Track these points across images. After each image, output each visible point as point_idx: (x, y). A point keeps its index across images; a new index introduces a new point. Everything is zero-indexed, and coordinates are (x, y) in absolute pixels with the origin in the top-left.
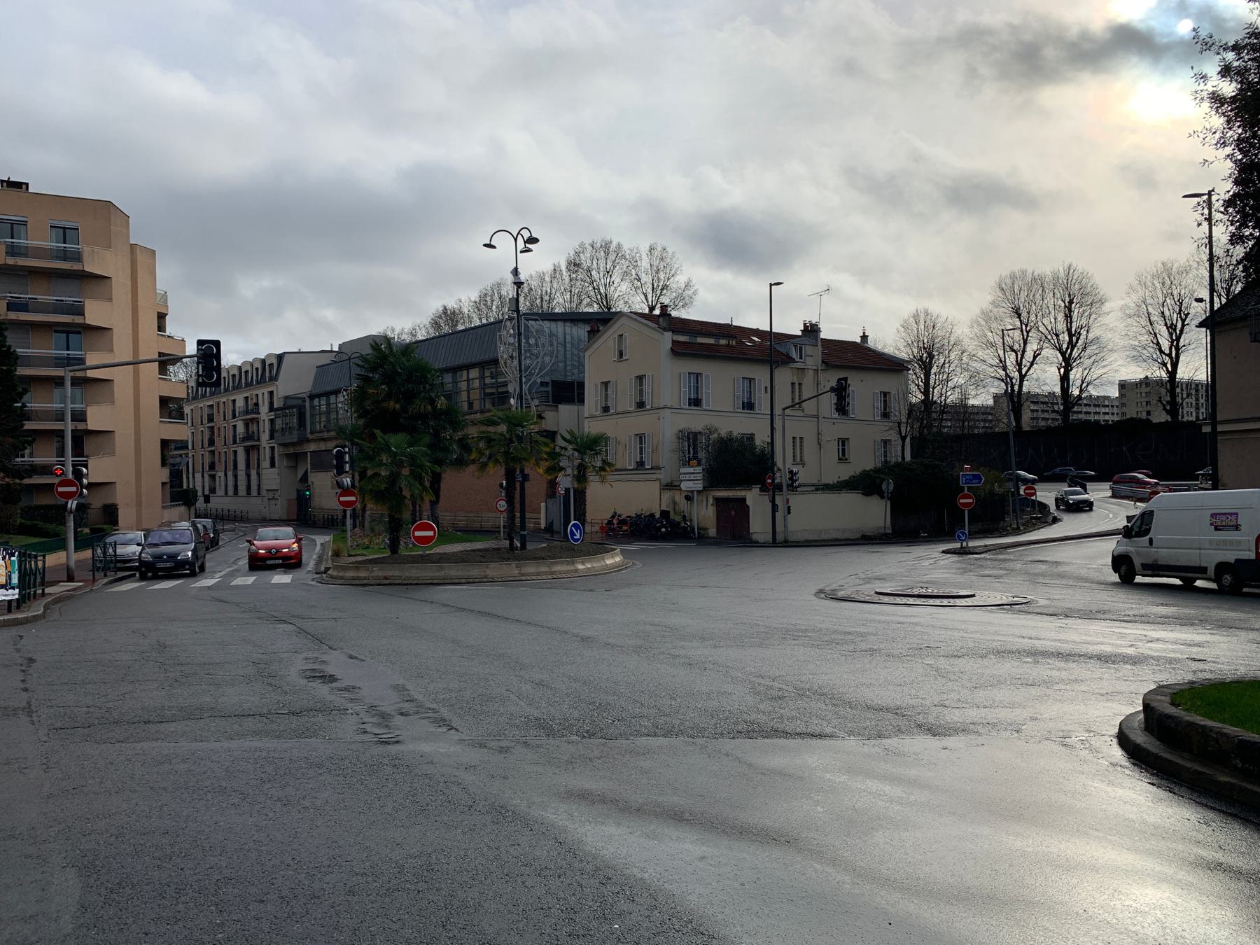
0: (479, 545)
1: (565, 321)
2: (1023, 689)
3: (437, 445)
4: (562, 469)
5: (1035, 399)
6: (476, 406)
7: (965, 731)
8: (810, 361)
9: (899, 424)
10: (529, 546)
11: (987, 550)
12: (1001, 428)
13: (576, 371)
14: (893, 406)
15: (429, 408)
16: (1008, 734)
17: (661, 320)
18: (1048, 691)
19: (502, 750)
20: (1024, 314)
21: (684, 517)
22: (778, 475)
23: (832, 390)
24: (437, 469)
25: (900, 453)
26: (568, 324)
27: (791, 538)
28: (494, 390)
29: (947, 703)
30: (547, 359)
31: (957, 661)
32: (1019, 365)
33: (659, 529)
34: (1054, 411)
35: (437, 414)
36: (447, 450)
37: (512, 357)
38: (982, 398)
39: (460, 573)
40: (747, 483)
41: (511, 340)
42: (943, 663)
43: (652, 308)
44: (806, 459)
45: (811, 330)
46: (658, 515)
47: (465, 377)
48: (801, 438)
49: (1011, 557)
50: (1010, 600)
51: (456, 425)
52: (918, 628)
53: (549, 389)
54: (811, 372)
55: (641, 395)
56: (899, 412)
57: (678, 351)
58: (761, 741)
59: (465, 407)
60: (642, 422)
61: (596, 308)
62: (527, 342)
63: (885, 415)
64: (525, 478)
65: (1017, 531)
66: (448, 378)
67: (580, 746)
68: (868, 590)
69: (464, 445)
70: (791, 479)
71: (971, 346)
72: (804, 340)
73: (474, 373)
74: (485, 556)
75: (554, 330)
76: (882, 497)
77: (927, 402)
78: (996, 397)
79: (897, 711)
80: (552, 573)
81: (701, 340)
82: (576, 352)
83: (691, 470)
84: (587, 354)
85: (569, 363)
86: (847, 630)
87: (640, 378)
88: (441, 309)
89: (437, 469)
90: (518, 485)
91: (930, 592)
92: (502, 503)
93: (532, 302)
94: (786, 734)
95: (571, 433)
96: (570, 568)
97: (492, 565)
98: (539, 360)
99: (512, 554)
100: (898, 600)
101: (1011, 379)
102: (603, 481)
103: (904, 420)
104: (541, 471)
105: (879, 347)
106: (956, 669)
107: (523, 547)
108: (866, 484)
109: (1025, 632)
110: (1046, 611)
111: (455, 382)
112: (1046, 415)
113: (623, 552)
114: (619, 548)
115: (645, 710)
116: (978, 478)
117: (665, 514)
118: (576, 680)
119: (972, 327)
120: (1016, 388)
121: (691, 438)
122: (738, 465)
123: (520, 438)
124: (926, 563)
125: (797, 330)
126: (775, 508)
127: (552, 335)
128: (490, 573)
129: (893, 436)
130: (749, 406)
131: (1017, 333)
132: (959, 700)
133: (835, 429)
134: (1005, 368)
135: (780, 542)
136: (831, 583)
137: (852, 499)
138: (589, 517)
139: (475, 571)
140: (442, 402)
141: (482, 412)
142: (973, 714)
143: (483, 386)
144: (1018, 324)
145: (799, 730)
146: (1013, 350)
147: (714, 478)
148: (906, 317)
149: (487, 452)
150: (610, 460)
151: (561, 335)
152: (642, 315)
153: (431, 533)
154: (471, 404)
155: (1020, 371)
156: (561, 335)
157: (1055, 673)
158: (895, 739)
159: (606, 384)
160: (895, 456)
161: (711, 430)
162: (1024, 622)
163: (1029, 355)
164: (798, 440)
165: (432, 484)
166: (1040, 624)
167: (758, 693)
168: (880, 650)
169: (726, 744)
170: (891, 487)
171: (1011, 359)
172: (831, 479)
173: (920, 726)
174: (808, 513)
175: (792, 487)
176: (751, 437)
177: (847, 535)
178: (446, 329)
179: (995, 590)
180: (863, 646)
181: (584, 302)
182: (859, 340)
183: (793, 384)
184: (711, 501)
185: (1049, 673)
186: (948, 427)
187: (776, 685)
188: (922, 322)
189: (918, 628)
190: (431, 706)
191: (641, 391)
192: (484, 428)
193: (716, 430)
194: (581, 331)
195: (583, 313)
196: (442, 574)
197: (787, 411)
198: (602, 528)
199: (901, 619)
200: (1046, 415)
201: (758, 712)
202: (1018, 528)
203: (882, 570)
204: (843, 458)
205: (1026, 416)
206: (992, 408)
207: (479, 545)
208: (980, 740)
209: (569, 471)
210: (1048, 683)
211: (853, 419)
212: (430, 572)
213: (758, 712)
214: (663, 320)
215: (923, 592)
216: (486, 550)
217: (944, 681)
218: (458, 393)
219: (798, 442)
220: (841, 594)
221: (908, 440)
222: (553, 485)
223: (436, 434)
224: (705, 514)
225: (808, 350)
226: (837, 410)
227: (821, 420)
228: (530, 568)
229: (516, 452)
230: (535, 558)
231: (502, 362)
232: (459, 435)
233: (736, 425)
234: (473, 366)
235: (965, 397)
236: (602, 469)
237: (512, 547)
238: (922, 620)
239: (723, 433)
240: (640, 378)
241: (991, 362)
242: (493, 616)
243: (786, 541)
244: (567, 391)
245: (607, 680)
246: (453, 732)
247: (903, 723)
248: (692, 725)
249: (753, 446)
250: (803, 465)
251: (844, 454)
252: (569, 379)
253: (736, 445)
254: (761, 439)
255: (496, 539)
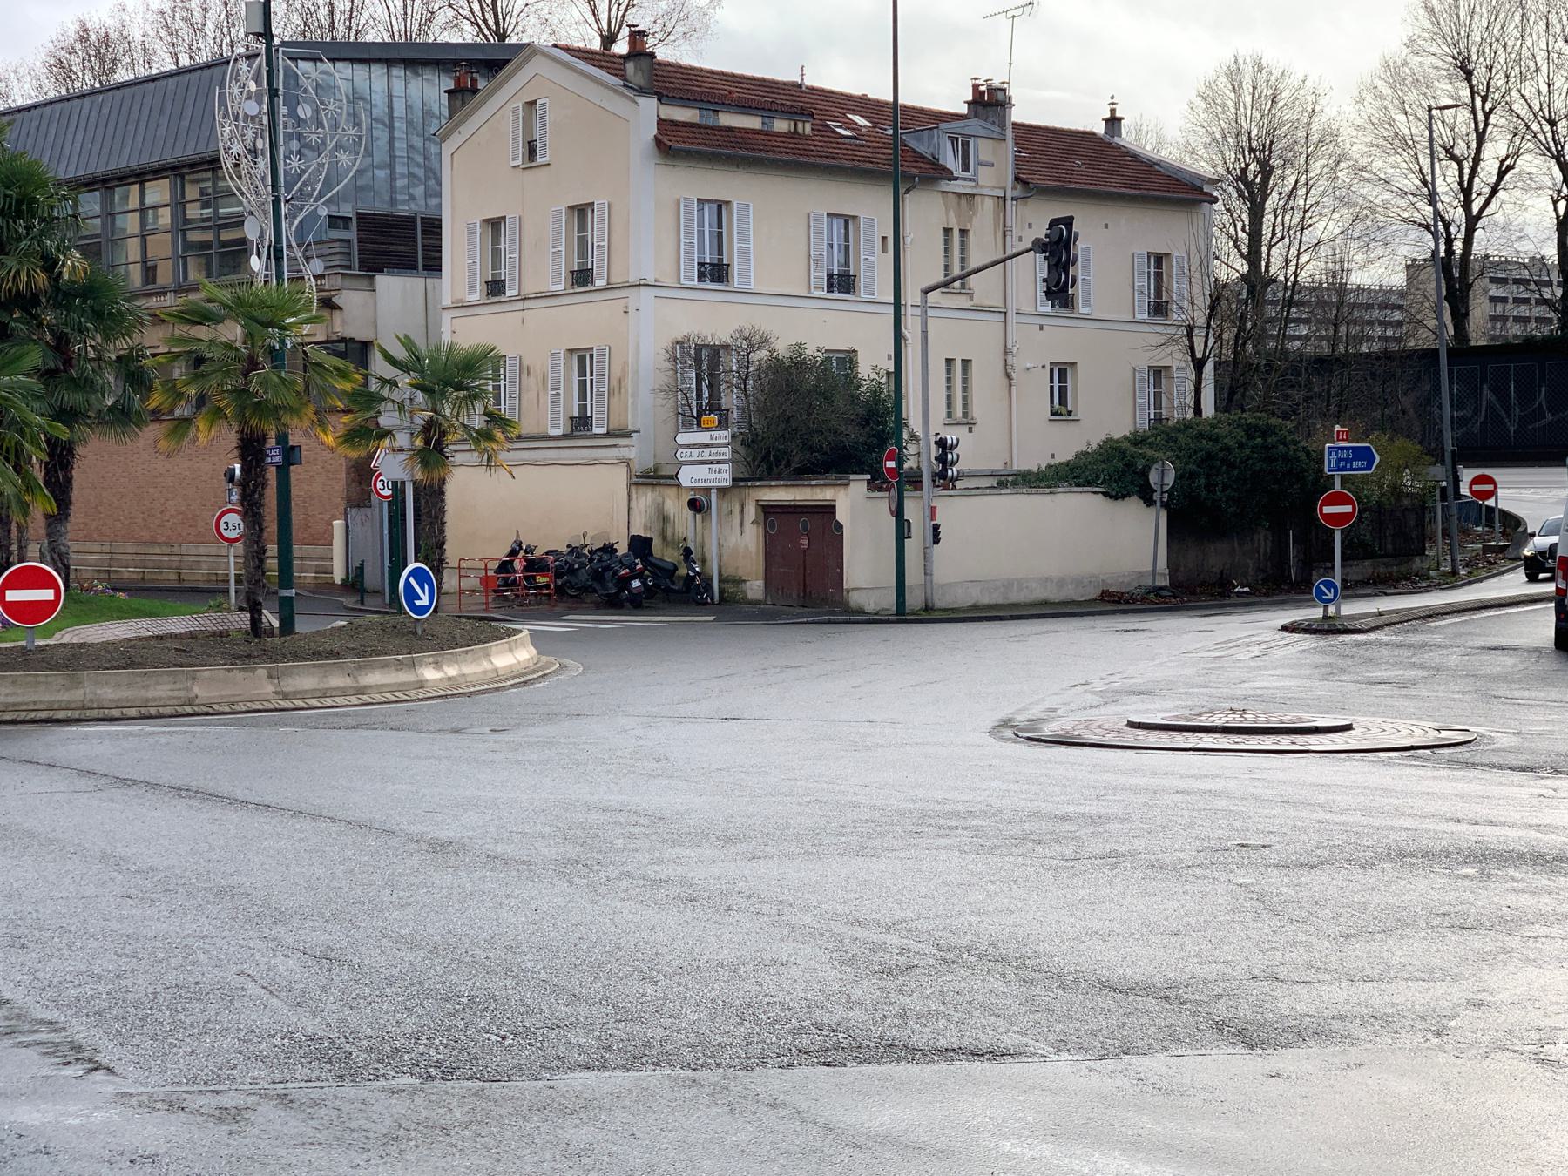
0: (174, 625)
1: (389, 63)
2: (1453, 938)
3: (61, 368)
4: (385, 434)
5: (1501, 273)
6: (164, 276)
7: (1321, 1034)
8: (986, 177)
9: (1190, 330)
10: (303, 626)
11: (1384, 622)
12: (1421, 340)
13: (419, 191)
14: (1178, 288)
15: (42, 278)
16: (1417, 1039)
17: (630, 66)
18: (1512, 942)
19: (225, 1115)
20: (1480, 74)
21: (687, 552)
22: (912, 449)
23: (1039, 246)
24: (62, 432)
25: (1190, 400)
26: (398, 72)
27: (938, 604)
28: (209, 236)
29: (1282, 972)
30: (344, 158)
31: (1307, 877)
32: (1467, 191)
33: (624, 582)
34: (1543, 301)
35: (62, 295)
36: (86, 385)
37: (253, 152)
38: (1379, 270)
39: (123, 694)
40: (838, 462)
41: (251, 108)
42: (1277, 883)
43: (609, 39)
44: (976, 412)
45: (989, 102)
46: (622, 548)
47: (134, 202)
48: (966, 362)
49: (1437, 638)
50: (1432, 737)
51: (110, 321)
52: (1221, 804)
53: (352, 234)
54: (989, 204)
55: (496, 263)
56: (1191, 303)
57: (672, 145)
58: (853, 1070)
59: (136, 276)
60: (583, 320)
61: (468, 34)
62: (292, 113)
63: (1159, 309)
64: (291, 455)
65: (1452, 580)
66: (91, 203)
67: (418, 1100)
68: (1110, 720)
69: (133, 373)
70: (942, 459)
71: (1357, 146)
72: (973, 126)
73: (158, 192)
74: (184, 652)
76: (1149, 502)
77: (1256, 280)
78: (1412, 267)
79: (1167, 993)
80: (361, 691)
81: (727, 120)
82: (418, 142)
83: (704, 437)
84: (447, 149)
85: (400, 169)
86: (1061, 810)
87: (581, 212)
88: (73, 29)
89: (62, 432)
90: (271, 474)
91: (1249, 721)
92: (234, 518)
93: (308, 15)
94: (913, 1053)
95: (407, 343)
96: (405, 677)
97: (206, 672)
98: (324, 159)
99: (263, 642)
100: (1180, 740)
101: (1447, 225)
102: (490, 462)
103: (1201, 320)
104: (329, 440)
105: (1147, 147)
106: (1306, 894)
107: (287, 626)
108: (1113, 472)
109: (1462, 809)
110: (1511, 760)
111: (109, 215)
112: (1523, 311)
113: (536, 638)
114: (526, 630)
115: (582, 1011)
116: (1365, 455)
117: (640, 545)
118: (413, 944)
119: (1361, 100)
120: (1458, 246)
121: (703, 363)
122: (816, 428)
123: (276, 356)
124: (1244, 655)
125: (955, 100)
126: (902, 530)
127: (355, 97)
128: (201, 691)
129: (1177, 359)
130: (842, 283)
131: (1464, 115)
132: (1309, 965)
133: (1044, 339)
134: (1432, 198)
135: (912, 611)
136: (1026, 705)
137: (1080, 509)
138: (452, 552)
139: (162, 689)
140: (73, 265)
141: (179, 291)
142: (1339, 996)
143: (182, 226)
144: (1465, 94)
145: (942, 1043)
146: (1453, 157)
147: (763, 457)
148: (1211, 75)
149: (192, 392)
150: (505, 410)
151: (379, 100)
153: (47, 595)
154: (150, 272)
155: (1467, 205)
156: (379, 100)
157: (1527, 900)
158: (1162, 1056)
159: (495, 224)
160: (1178, 407)
161: (753, 341)
162: (1461, 786)
163: (1489, 169)
164: (958, 364)
165: (49, 472)
166: (1496, 791)
167: (850, 961)
168: (1134, 854)
169: (771, 1081)
170: (1170, 479)
171: (1447, 180)
172: (1032, 460)
173: (1218, 1026)
174: (982, 537)
175: (944, 478)
176: (848, 359)
177: (1070, 593)
178: (87, 81)
179: (1400, 715)
180: (1095, 847)
181: (440, 19)
182: (1100, 129)
184: (751, 512)
185: (1512, 899)
186: (1303, 337)
187: (893, 940)
188: (1247, 88)
189: (1221, 804)
190: (47, 1016)
191: (582, 242)
192: (182, 330)
193: (764, 341)
194: (433, 90)
195: (436, 46)
196: (77, 695)
197: (933, 297)
198: (485, 580)
199: (1182, 784)
200: (1523, 311)
201: (850, 1003)
202: (1454, 573)
203: (1144, 672)
204: (1061, 410)
205: (1479, 311)
206: (1402, 294)
207: (174, 625)
208: (1355, 1054)
209: (402, 440)
210: (1510, 922)
211: (1086, 318)
212: (46, 691)
213: (850, 1003)
214: (634, 66)
215: (1236, 720)
216: (192, 636)
217: (1276, 922)
218: (115, 241)
219: (959, 370)
220: (1048, 730)
221: (1209, 368)
222: (363, 473)
223: (61, 345)
224: (736, 545)
225: (983, 149)
226: (1049, 294)
228: (305, 679)
229: (261, 398)
230: (317, 655)
231: (228, 163)
232: (122, 345)
233: (812, 328)
234: (157, 173)
235: (1341, 266)
236: (485, 435)
237: (256, 626)
238: (1232, 784)
239: (782, 348)
240: (581, 212)
241: (1409, 187)
242: (209, 796)
243: (928, 608)
244: (398, 242)
245: (491, 942)
246: (99, 1076)
247: (1181, 1020)
248: (693, 1039)
249: (852, 380)
250: (971, 426)
251: (1063, 401)
252: (402, 210)
253: (812, 377)
254: (872, 364)
255: (219, 608)
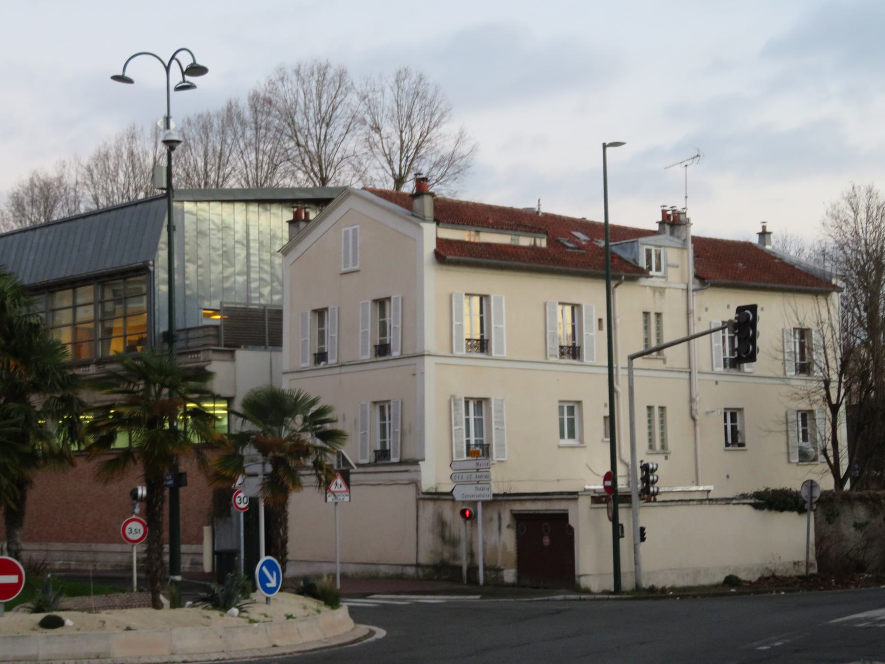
1: (247, 202)
26: (254, 208)
43: (400, 181)
47: (67, 302)
48: (662, 409)
60: (382, 379)
63: (804, 368)
73: (86, 294)
75: (228, 219)
85: (253, 275)
87: (381, 303)
105: (791, 253)
126: (618, 532)
130: (574, 352)
151: (239, 227)
152: (384, 194)
159: (320, 313)
164: (657, 412)
182: (755, 240)
183: (646, 314)
184: (507, 519)
197: (637, 362)
214: (411, 198)
219: (657, 415)
221: (842, 409)
227: (696, 377)
